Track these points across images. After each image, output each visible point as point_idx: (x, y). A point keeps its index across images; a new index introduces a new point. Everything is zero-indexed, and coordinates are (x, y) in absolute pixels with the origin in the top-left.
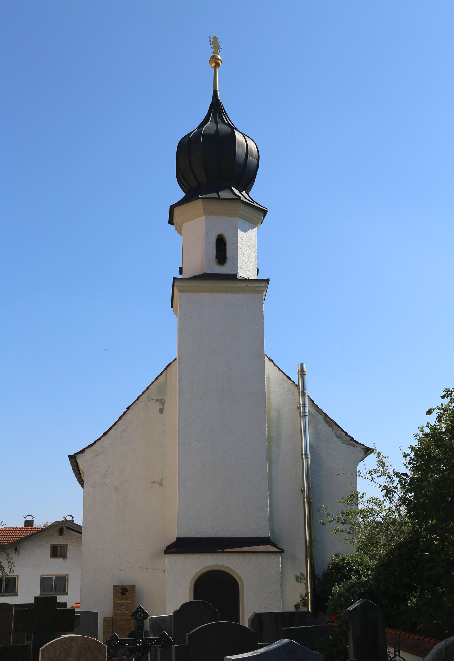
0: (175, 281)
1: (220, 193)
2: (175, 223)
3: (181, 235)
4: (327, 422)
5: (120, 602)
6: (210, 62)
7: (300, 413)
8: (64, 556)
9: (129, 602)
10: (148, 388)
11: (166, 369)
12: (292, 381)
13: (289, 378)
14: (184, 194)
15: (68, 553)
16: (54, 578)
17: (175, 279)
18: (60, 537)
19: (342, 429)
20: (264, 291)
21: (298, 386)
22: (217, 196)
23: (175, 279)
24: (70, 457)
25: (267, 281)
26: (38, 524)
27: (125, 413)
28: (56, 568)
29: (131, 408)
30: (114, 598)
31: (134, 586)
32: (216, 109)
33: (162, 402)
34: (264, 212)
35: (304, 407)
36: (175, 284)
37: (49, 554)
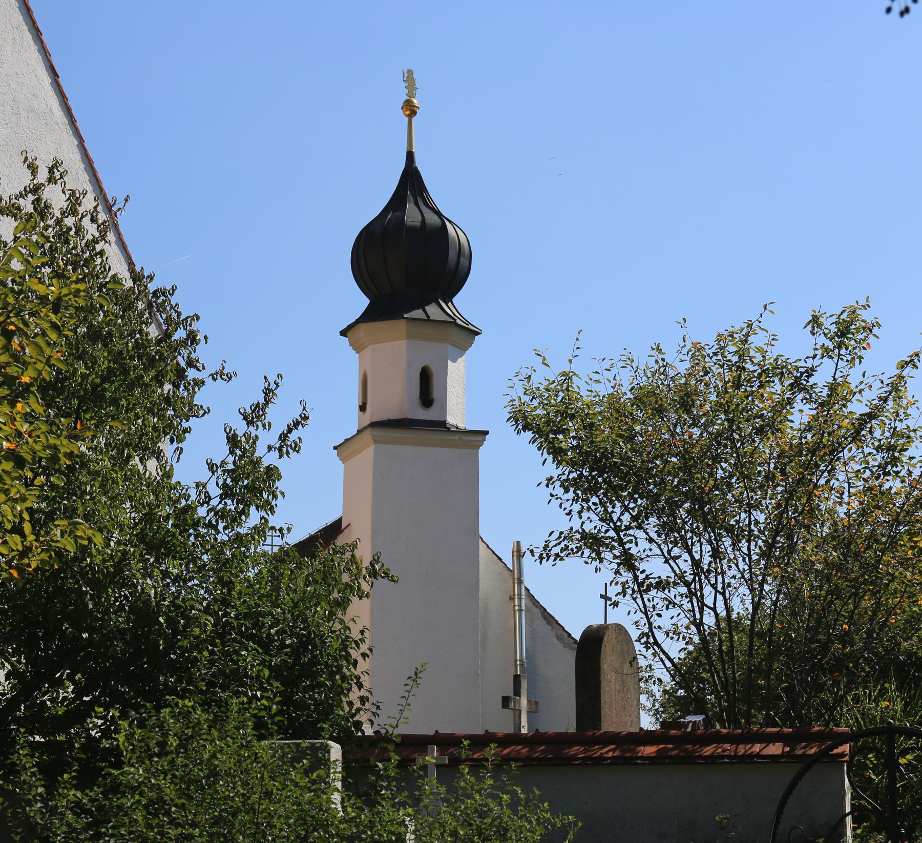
1: (426, 308)
4: (546, 619)
7: (514, 606)
13: (500, 559)
19: (563, 628)
21: (512, 571)
32: (411, 182)
35: (520, 599)
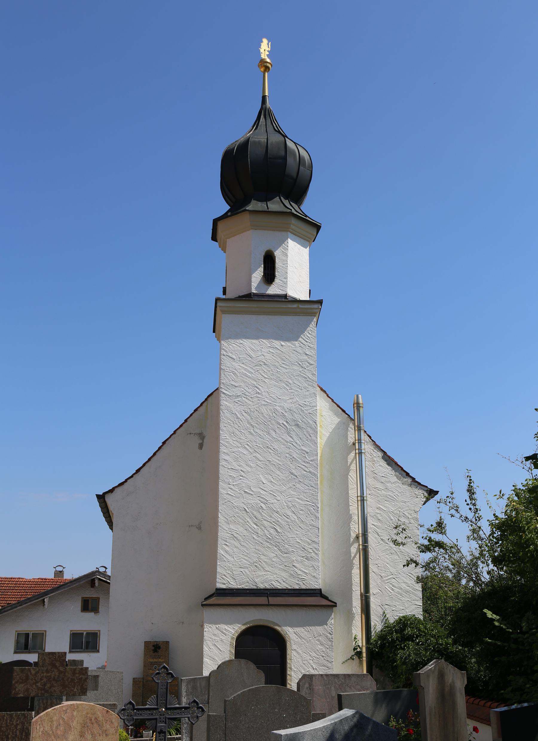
0: (218, 302)
2: (218, 239)
3: (225, 252)
5: (151, 660)
6: (259, 66)
8: (96, 610)
9: (162, 661)
10: (186, 421)
11: (206, 399)
12: (346, 414)
14: (228, 208)
15: (100, 606)
16: (84, 634)
17: (217, 300)
18: (92, 589)
20: (316, 313)
21: (354, 420)
22: (265, 209)
23: (217, 300)
24: (98, 496)
25: (320, 302)
26: (68, 576)
27: (160, 448)
28: (86, 623)
29: (167, 442)
30: (145, 656)
31: (167, 643)
32: (264, 112)
33: (202, 436)
34: (318, 227)
36: (218, 304)
37: (80, 608)
